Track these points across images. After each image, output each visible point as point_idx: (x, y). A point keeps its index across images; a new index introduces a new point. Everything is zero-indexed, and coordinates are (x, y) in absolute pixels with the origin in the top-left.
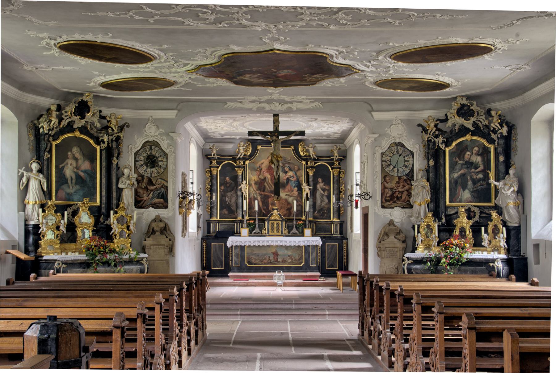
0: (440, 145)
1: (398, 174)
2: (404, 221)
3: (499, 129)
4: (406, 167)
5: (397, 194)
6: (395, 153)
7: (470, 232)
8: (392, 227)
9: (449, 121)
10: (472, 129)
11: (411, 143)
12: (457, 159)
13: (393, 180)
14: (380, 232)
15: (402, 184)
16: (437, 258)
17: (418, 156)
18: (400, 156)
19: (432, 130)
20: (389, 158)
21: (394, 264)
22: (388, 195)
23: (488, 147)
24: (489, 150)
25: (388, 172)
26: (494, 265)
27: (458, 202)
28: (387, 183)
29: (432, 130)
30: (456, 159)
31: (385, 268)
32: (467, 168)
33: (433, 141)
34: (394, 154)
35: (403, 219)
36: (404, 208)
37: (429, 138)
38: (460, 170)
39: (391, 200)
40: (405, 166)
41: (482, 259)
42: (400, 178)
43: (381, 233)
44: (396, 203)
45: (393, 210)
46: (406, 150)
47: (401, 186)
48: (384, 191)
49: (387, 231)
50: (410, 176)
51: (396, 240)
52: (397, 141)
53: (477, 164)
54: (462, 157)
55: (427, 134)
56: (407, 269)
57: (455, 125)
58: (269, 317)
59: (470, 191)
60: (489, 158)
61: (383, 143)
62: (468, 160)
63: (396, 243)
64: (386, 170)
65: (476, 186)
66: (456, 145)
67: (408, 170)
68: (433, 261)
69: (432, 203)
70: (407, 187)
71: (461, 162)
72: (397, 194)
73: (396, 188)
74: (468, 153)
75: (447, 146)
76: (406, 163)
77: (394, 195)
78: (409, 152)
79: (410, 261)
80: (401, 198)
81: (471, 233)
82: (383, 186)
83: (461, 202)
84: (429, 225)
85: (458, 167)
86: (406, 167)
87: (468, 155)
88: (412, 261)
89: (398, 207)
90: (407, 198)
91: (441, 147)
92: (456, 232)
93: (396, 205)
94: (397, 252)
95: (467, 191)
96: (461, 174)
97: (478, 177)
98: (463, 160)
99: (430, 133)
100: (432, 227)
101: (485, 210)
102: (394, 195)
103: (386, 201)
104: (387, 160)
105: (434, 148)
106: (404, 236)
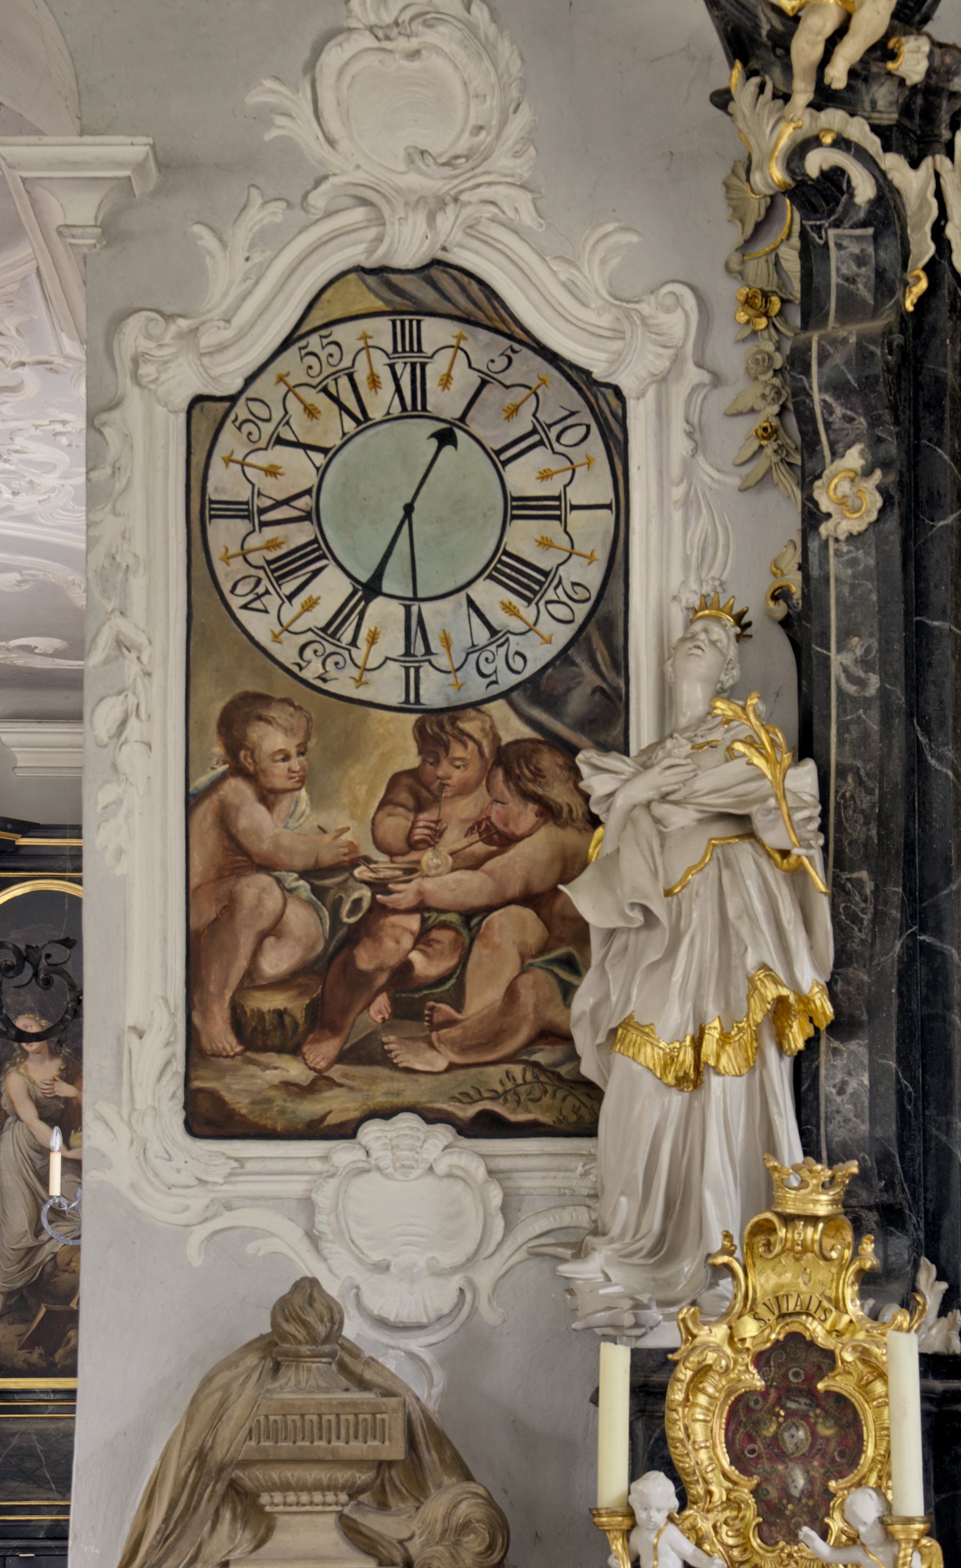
1: (412, 683)
2: (489, 1314)
17: (680, 445)
18: (445, 438)
25: (286, 653)
28: (268, 797)
34: (363, 420)
35: (485, 1276)
44: (385, 1059)
47: (453, 838)
48: (230, 906)
50: (577, 702)
69: (858, 1047)
73: (384, 867)
77: (364, 959)
89: (407, 1122)
102: (364, 959)
104: (276, 489)
106: (464, 1509)
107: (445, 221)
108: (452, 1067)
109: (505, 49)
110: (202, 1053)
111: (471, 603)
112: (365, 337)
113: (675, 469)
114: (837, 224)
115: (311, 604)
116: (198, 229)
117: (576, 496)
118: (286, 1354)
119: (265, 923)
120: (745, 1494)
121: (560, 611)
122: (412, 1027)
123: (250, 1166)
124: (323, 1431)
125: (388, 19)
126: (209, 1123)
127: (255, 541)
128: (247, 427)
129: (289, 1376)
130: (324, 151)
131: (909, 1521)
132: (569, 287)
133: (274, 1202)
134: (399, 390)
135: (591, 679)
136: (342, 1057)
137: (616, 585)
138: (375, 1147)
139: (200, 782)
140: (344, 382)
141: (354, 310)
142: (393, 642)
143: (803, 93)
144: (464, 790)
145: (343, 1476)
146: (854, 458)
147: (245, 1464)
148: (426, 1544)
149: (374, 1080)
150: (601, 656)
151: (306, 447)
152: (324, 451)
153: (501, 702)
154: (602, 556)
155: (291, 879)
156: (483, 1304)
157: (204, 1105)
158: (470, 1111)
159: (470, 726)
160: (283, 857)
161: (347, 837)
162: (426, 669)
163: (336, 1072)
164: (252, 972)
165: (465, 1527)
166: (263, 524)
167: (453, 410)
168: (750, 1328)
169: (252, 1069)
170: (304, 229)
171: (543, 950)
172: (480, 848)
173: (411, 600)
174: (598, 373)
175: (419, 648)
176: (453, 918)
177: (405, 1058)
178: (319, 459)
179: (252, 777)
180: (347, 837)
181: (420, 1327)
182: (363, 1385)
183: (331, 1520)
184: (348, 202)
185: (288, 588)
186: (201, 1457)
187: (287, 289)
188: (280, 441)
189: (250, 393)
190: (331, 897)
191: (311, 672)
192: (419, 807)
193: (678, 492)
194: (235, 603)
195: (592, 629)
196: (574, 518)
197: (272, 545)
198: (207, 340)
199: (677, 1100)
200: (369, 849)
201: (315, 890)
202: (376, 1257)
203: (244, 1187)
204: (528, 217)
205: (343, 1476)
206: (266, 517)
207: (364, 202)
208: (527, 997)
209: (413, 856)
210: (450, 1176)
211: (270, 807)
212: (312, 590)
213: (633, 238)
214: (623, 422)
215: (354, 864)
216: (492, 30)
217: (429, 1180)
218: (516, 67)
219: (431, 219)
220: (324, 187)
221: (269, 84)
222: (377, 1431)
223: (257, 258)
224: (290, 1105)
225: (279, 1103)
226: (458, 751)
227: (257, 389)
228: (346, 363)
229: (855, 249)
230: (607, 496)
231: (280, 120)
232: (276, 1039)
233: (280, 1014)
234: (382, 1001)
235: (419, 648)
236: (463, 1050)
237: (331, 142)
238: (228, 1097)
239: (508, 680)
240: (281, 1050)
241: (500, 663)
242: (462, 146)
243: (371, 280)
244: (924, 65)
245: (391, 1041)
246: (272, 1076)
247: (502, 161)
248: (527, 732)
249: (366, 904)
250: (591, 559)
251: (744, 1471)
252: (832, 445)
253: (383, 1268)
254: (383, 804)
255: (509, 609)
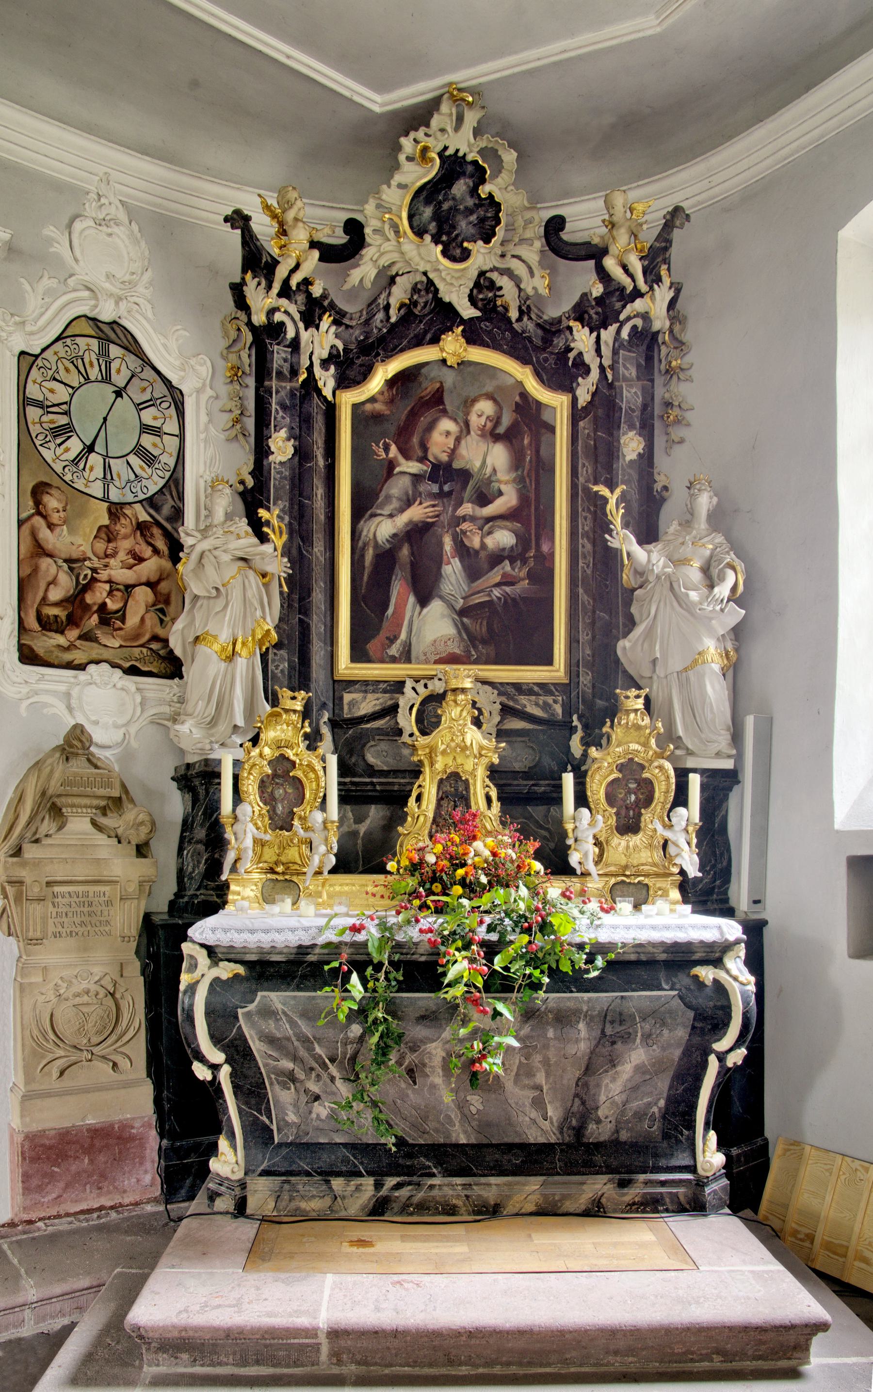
0: (318, 371)
1: (106, 490)
2: (134, 744)
3: (637, 294)
4: (150, 459)
5: (98, 595)
6: (94, 373)
7: (489, 800)
8: (79, 766)
9: (368, 253)
10: (468, 312)
11: (173, 345)
12: (394, 450)
13: (82, 513)
14: (10, 793)
15: (125, 545)
16: (398, 947)
17: (204, 418)
18: (119, 394)
19: (297, 267)
20: (62, 394)
21: (98, 971)
22: (55, 595)
23: (539, 404)
24: (546, 416)
25: (58, 467)
26: (722, 975)
27: (394, 660)
28: (51, 526)
29: (297, 267)
30: (387, 449)
31: (51, 996)
32: (441, 495)
33: (291, 334)
34: (87, 379)
35: (133, 730)
36: (133, 671)
37: (272, 311)
38: (408, 503)
39: (73, 621)
40: (139, 451)
41: (654, 945)
42: (116, 510)
43: (20, 799)
44: (95, 640)
45: (82, 676)
46: (148, 373)
47: (122, 556)
48: (36, 570)
49: (54, 787)
50: (166, 510)
51: (101, 839)
52: (106, 314)
53: (489, 481)
54: (415, 440)
55: (269, 287)
56: (210, 1013)
57: (392, 280)
58: (623, 32)
59: (451, 607)
60: (543, 452)
61: (33, 303)
62: (444, 458)
63: (103, 854)
64: (48, 455)
65: (480, 583)
66: (391, 383)
67: (154, 484)
68: (378, 967)
69: (283, 653)
70: (151, 566)
71: (413, 467)
72: (98, 595)
73: (96, 563)
74: (446, 425)
75: (344, 382)
76: (148, 441)
77: (89, 598)
78: (160, 390)
79: (226, 971)
80: (123, 620)
81: (496, 805)
82: (27, 541)
83: (408, 660)
84: (283, 758)
85: (397, 487)
86: (150, 459)
87: (448, 433)
88: (240, 970)
89: (105, 666)
90: (152, 620)
91: (320, 384)
92: (419, 799)
93: (95, 651)
94: (109, 903)
95: (436, 606)
96: (410, 522)
97: (490, 542)
98: (423, 459)
99: (286, 282)
100: (298, 773)
101: (523, 700)
102: (89, 598)
103: (47, 624)
104: (54, 399)
105: (294, 372)
106: (141, 817)
107: (123, 305)
108: (121, 646)
109: (143, 244)
110: (25, 629)
111: (128, 463)
112: (88, 345)
113: (202, 427)
114: (278, 344)
115: (67, 450)
116: (22, 280)
117: (166, 429)
118: (72, 753)
119: (50, 579)
120: (264, 812)
121: (160, 473)
122: (106, 629)
123: (46, 677)
124: (89, 784)
125: (101, 217)
126: (27, 658)
127: (45, 418)
128: (42, 370)
129: (73, 762)
130: (73, 263)
131: (333, 822)
132: (165, 346)
133: (54, 693)
134: (100, 370)
135: (172, 503)
136: (80, 637)
137: (180, 467)
138: (95, 674)
139: (24, 515)
140: (80, 361)
141: (84, 333)
142: (99, 472)
143: (276, 287)
144: (126, 537)
145: (96, 802)
146: (283, 433)
147: (59, 796)
148: (125, 830)
149: (92, 648)
150: (174, 493)
151: (65, 384)
152: (73, 388)
153: (139, 505)
154: (175, 455)
155: (60, 562)
156: (132, 741)
157: (26, 651)
158: (127, 665)
159: (128, 511)
160: (57, 552)
161: (82, 548)
162: (111, 485)
163: (78, 643)
164: (44, 599)
165: (142, 823)
166: (48, 412)
167: (122, 384)
168: (267, 751)
169: (45, 638)
170: (64, 294)
171: (153, 605)
172: (132, 561)
173: (106, 457)
174: (174, 383)
175: (109, 477)
176: (121, 587)
177: (104, 640)
178: (71, 391)
179: (45, 517)
180: (82, 548)
181: (110, 747)
182: (96, 767)
183: (88, 819)
184: (82, 287)
185: (59, 441)
186: (44, 793)
187: (59, 316)
188: (55, 379)
189: (43, 356)
190: (76, 572)
191: (68, 478)
192: (109, 541)
193: (203, 436)
194: (38, 443)
195: (171, 483)
196: (165, 437)
197: (52, 422)
198: (29, 328)
199: (223, 665)
200: (90, 554)
201: (70, 568)
202: (93, 718)
203: (41, 686)
204: (150, 314)
205: (96, 802)
206: (50, 410)
207: (89, 289)
208: (148, 623)
209: (107, 560)
210: (122, 689)
211: (52, 530)
212: (68, 444)
213: (187, 334)
214: (183, 404)
215: (85, 560)
216: (139, 235)
217: (114, 690)
218: (147, 253)
219: (117, 303)
220: (73, 278)
221: (52, 228)
222: (109, 785)
223: (47, 300)
224: (60, 655)
225: (56, 653)
226: (123, 521)
227: (45, 355)
228: (81, 354)
229: (284, 355)
230: (177, 432)
231: (56, 245)
232: (54, 627)
233: (56, 617)
234: (95, 617)
235: (109, 477)
236: (125, 640)
237: (76, 260)
238: (35, 648)
239: (142, 497)
240: (56, 632)
241: (139, 489)
242: (127, 278)
243: (91, 322)
244: (321, 291)
245: (99, 633)
246: (53, 642)
247: (140, 289)
248: (149, 519)
249: (89, 577)
250: (171, 456)
251: (265, 804)
252: (275, 426)
253: (96, 723)
254: (95, 537)
255: (141, 467)
